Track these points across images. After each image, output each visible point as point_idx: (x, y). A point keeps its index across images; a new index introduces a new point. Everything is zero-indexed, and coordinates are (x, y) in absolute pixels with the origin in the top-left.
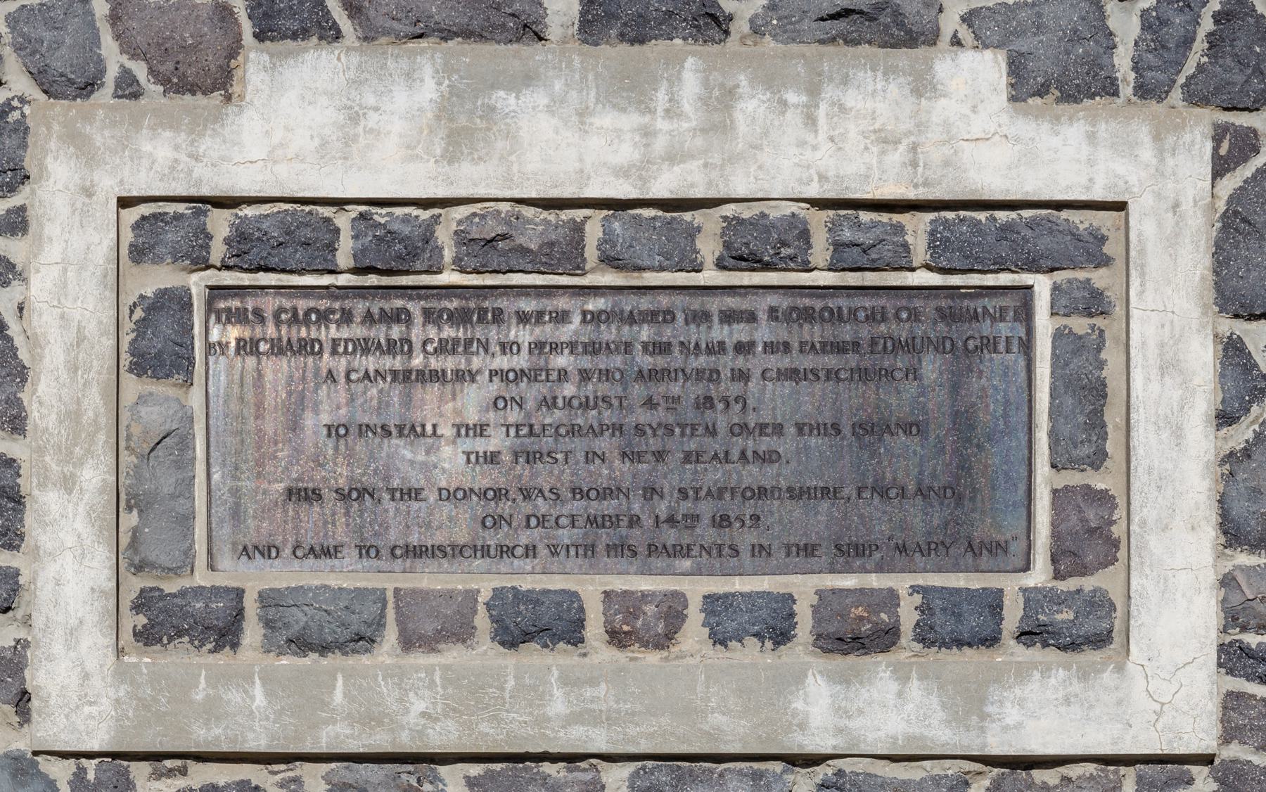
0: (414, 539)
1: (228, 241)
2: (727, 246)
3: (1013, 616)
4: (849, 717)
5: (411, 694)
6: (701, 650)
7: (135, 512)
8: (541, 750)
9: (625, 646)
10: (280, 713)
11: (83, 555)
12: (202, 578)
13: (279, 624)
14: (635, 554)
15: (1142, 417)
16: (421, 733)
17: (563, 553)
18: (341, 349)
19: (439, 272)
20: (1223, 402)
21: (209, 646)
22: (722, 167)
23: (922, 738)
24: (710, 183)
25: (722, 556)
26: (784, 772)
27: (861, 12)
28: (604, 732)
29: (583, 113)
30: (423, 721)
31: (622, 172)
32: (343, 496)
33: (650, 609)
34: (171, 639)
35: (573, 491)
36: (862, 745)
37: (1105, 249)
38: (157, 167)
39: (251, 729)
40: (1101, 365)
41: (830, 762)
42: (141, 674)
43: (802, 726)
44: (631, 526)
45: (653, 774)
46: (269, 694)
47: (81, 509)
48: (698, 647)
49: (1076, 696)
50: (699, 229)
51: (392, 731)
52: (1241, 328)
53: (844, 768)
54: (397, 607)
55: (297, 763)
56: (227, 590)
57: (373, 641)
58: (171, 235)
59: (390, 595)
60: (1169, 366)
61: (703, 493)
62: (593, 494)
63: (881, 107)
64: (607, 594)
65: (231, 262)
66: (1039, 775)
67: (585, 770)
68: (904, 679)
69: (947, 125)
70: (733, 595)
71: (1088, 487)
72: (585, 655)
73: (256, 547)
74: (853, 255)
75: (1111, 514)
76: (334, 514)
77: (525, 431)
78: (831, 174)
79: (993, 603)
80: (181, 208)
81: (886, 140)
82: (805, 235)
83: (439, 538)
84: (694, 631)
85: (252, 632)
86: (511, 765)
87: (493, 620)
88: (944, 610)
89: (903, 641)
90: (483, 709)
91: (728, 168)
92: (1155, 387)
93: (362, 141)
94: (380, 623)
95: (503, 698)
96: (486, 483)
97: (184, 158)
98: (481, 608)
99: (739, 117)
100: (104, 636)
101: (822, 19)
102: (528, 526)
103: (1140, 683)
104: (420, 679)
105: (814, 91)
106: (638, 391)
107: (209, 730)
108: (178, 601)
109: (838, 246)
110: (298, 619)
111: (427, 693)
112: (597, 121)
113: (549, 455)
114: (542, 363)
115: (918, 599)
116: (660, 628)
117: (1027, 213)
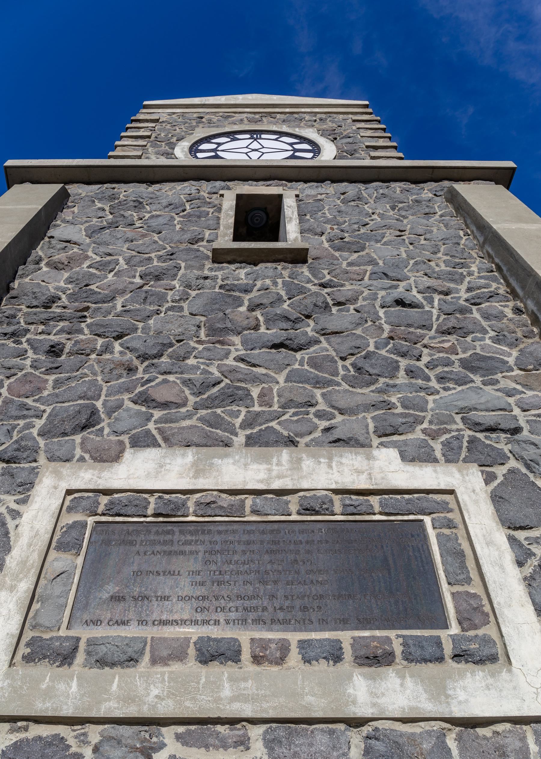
0: (164, 617)
1: (106, 505)
2: (301, 505)
3: (448, 649)
4: (378, 697)
5: (152, 686)
6: (298, 666)
7: (40, 603)
8: (216, 716)
9: (261, 664)
10: (83, 696)
11: (9, 619)
12: (63, 633)
13: (94, 653)
14: (265, 623)
15: (485, 561)
16: (154, 707)
17: (232, 623)
18: (144, 544)
19: (187, 516)
20: (516, 557)
21: (57, 664)
22: (298, 480)
23: (417, 708)
24: (294, 485)
25: (304, 624)
26: (345, 730)
27: (344, 440)
28: (250, 706)
29: (246, 465)
30: (156, 700)
31: (261, 481)
32: (135, 599)
33: (273, 646)
34: (40, 660)
35: (238, 597)
36: (387, 713)
37: (449, 506)
38: (84, 480)
39: (66, 704)
40: (460, 545)
41: (370, 723)
42: (18, 674)
43: (354, 702)
44: (263, 611)
45: (275, 731)
46: (79, 685)
47: (14, 599)
48: (296, 664)
49: (492, 685)
50: (290, 501)
51: (139, 705)
52: (512, 532)
53: (378, 726)
54: (152, 645)
55: (87, 725)
56: (73, 637)
57: (137, 661)
58: (84, 503)
59: (149, 640)
60: (489, 543)
61: (295, 598)
62: (246, 598)
63: (355, 463)
64: (252, 640)
65: (106, 512)
66: (481, 731)
67: (239, 729)
68: (403, 677)
69: (381, 468)
70: (312, 640)
71: (467, 592)
72: (241, 668)
73: (91, 621)
74: (351, 509)
75: (481, 603)
76: (129, 607)
77: (217, 573)
78: (340, 481)
79: (438, 642)
80: (90, 494)
81: (359, 472)
82: (331, 501)
83: (176, 617)
84: (294, 657)
85: (80, 657)
86: (200, 727)
87: (198, 650)
88: (414, 645)
89: (397, 660)
90: (188, 694)
91: (300, 480)
92: (486, 550)
93: (163, 473)
94: (142, 652)
95: (199, 688)
96: (199, 593)
97: (95, 478)
98: (192, 645)
99: (303, 465)
100: (6, 655)
101: (330, 443)
102: (217, 611)
103: (522, 678)
104: (157, 678)
105: (330, 459)
106: (267, 557)
107: (44, 704)
108: (48, 642)
109: (345, 506)
110: (103, 650)
111: (160, 685)
112: (251, 467)
113: (227, 582)
114: (226, 548)
115: (401, 640)
116: (278, 655)
117: (416, 495)
